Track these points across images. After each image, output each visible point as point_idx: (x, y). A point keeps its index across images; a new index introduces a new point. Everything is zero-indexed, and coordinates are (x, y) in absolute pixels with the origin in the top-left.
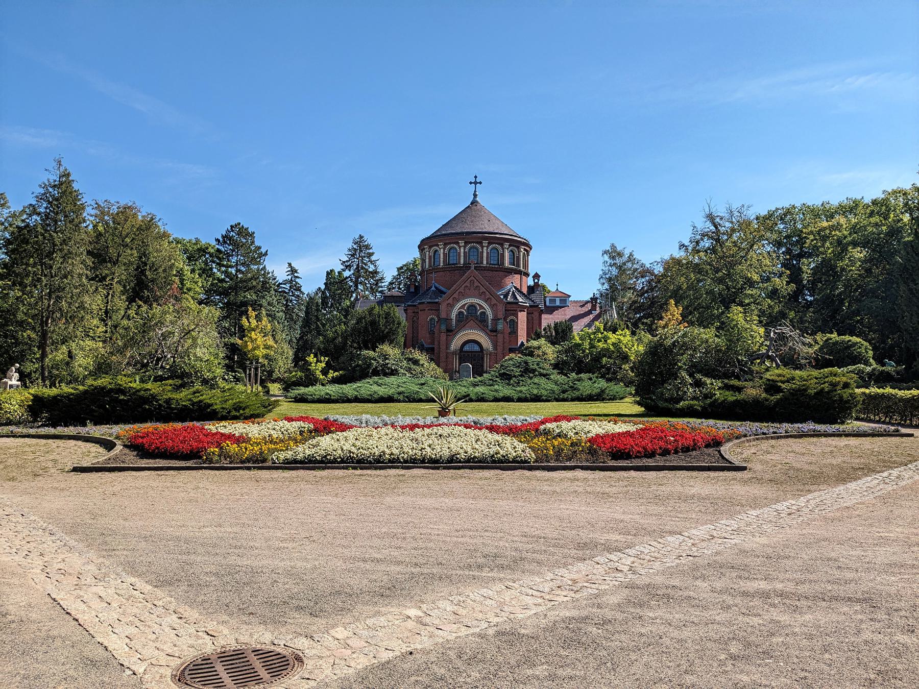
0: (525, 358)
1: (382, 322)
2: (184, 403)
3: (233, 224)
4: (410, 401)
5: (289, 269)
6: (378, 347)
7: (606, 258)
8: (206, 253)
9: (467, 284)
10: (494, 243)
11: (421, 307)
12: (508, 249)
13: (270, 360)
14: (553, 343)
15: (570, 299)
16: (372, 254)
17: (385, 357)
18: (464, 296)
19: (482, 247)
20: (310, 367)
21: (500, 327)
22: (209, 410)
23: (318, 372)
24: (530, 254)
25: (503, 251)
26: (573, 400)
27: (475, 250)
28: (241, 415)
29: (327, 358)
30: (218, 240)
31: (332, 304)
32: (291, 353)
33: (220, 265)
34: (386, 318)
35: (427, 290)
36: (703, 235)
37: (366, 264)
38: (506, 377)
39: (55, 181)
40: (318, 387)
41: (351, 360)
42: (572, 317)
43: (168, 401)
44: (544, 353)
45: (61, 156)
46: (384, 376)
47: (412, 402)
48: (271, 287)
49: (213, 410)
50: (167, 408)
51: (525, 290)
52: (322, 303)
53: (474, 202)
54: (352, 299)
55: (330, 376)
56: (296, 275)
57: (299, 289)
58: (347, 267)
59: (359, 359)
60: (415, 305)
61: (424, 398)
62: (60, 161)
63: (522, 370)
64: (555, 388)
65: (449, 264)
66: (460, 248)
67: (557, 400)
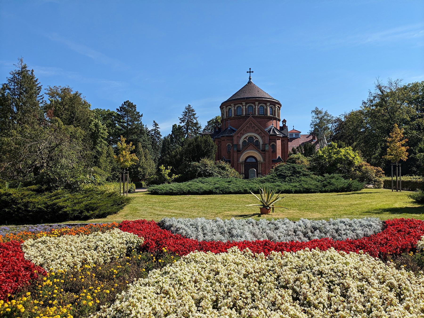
0: (292, 165)
1: (203, 145)
2: (40, 206)
3: (125, 101)
4: (223, 194)
5: (154, 124)
6: (201, 160)
7: (313, 114)
8: (112, 116)
9: (248, 125)
11: (222, 138)
12: (269, 106)
13: (144, 169)
14: (305, 155)
15: (301, 134)
16: (195, 114)
17: (205, 165)
18: (247, 132)
19: (255, 105)
20: (162, 173)
21: (267, 148)
22: (61, 212)
23: (166, 175)
24: (281, 109)
25: (267, 107)
26: (331, 191)
28: (92, 215)
29: (171, 167)
30: (118, 109)
31: (175, 141)
32: (154, 165)
33: (119, 122)
34: (205, 143)
35: (226, 130)
36: (375, 97)
37: (192, 120)
38: (282, 177)
39: (19, 71)
40: (166, 184)
41: (185, 167)
43: (26, 205)
44: (302, 162)
45: (22, 57)
46: (205, 177)
47: (225, 194)
48: (144, 132)
49: (64, 212)
50: (25, 210)
51: (278, 128)
52: (171, 141)
53: (250, 82)
54: (185, 137)
55: (173, 177)
56: (157, 126)
57: (159, 133)
58: (182, 121)
59: (190, 167)
60: (219, 138)
61: (232, 191)
62: (22, 60)
63: (292, 172)
64: (319, 184)
65: (237, 115)
66: (243, 106)
67: (321, 192)
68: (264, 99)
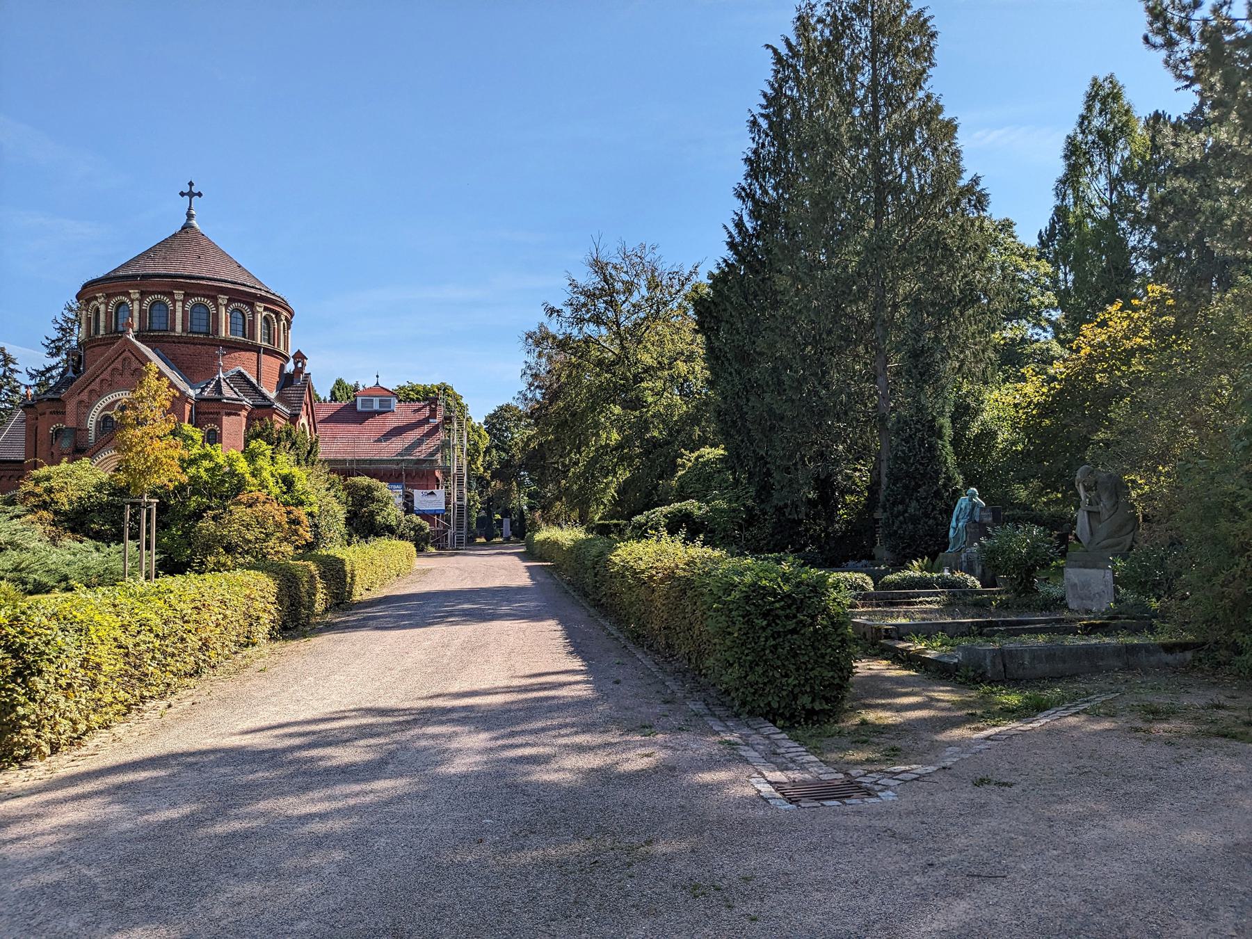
10: (198, 295)
19: (174, 302)
25: (217, 310)
27: (203, 310)
42: (395, 428)
53: (187, 227)
56: (11, 366)
68: (204, 282)
